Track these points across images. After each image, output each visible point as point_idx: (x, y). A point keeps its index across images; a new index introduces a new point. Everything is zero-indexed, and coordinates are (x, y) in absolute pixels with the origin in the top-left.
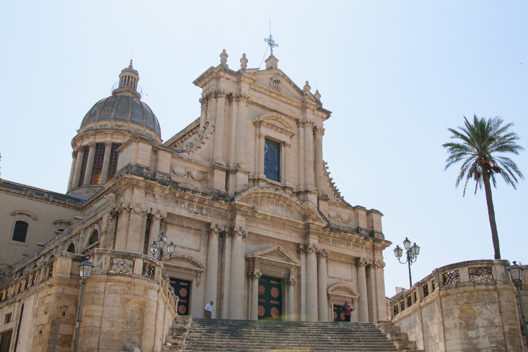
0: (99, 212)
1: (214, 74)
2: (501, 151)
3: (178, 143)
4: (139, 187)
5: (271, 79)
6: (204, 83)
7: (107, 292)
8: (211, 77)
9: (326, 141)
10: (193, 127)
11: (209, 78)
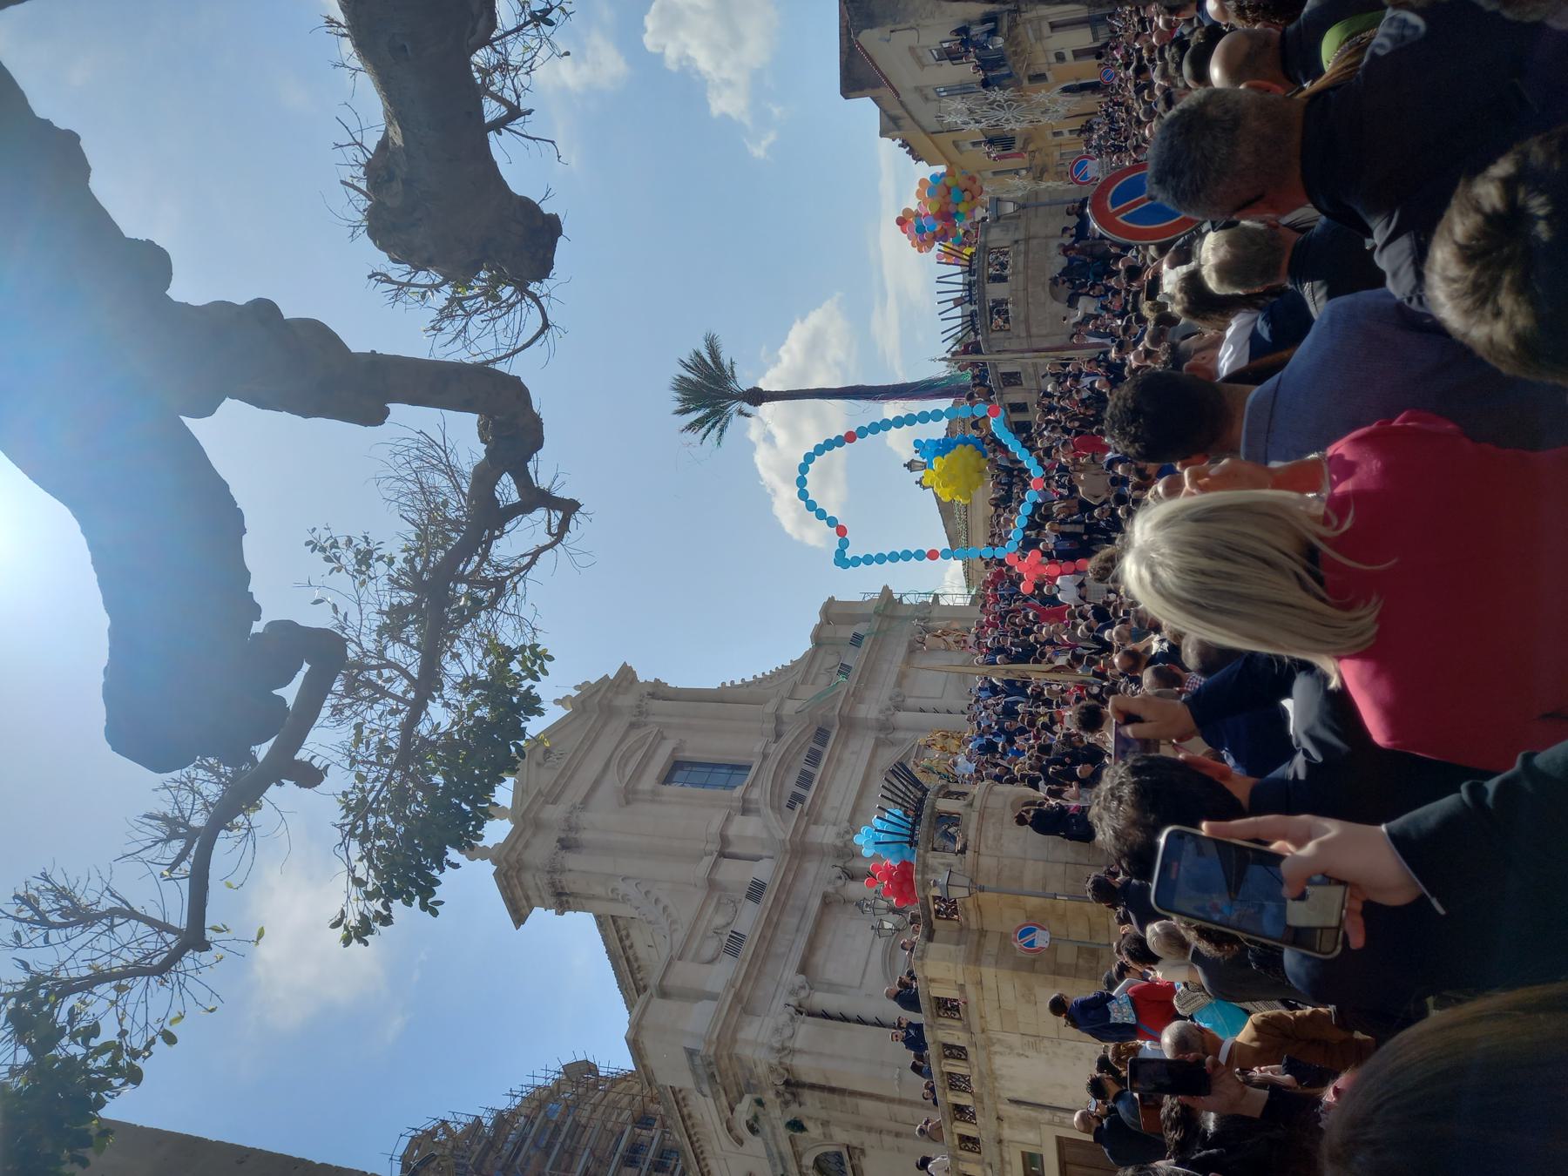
0: (778, 1147)
1: (509, 873)
2: (432, 1134)
3: (641, 979)
4: (735, 1031)
5: (539, 765)
6: (524, 902)
8: (516, 881)
9: (677, 679)
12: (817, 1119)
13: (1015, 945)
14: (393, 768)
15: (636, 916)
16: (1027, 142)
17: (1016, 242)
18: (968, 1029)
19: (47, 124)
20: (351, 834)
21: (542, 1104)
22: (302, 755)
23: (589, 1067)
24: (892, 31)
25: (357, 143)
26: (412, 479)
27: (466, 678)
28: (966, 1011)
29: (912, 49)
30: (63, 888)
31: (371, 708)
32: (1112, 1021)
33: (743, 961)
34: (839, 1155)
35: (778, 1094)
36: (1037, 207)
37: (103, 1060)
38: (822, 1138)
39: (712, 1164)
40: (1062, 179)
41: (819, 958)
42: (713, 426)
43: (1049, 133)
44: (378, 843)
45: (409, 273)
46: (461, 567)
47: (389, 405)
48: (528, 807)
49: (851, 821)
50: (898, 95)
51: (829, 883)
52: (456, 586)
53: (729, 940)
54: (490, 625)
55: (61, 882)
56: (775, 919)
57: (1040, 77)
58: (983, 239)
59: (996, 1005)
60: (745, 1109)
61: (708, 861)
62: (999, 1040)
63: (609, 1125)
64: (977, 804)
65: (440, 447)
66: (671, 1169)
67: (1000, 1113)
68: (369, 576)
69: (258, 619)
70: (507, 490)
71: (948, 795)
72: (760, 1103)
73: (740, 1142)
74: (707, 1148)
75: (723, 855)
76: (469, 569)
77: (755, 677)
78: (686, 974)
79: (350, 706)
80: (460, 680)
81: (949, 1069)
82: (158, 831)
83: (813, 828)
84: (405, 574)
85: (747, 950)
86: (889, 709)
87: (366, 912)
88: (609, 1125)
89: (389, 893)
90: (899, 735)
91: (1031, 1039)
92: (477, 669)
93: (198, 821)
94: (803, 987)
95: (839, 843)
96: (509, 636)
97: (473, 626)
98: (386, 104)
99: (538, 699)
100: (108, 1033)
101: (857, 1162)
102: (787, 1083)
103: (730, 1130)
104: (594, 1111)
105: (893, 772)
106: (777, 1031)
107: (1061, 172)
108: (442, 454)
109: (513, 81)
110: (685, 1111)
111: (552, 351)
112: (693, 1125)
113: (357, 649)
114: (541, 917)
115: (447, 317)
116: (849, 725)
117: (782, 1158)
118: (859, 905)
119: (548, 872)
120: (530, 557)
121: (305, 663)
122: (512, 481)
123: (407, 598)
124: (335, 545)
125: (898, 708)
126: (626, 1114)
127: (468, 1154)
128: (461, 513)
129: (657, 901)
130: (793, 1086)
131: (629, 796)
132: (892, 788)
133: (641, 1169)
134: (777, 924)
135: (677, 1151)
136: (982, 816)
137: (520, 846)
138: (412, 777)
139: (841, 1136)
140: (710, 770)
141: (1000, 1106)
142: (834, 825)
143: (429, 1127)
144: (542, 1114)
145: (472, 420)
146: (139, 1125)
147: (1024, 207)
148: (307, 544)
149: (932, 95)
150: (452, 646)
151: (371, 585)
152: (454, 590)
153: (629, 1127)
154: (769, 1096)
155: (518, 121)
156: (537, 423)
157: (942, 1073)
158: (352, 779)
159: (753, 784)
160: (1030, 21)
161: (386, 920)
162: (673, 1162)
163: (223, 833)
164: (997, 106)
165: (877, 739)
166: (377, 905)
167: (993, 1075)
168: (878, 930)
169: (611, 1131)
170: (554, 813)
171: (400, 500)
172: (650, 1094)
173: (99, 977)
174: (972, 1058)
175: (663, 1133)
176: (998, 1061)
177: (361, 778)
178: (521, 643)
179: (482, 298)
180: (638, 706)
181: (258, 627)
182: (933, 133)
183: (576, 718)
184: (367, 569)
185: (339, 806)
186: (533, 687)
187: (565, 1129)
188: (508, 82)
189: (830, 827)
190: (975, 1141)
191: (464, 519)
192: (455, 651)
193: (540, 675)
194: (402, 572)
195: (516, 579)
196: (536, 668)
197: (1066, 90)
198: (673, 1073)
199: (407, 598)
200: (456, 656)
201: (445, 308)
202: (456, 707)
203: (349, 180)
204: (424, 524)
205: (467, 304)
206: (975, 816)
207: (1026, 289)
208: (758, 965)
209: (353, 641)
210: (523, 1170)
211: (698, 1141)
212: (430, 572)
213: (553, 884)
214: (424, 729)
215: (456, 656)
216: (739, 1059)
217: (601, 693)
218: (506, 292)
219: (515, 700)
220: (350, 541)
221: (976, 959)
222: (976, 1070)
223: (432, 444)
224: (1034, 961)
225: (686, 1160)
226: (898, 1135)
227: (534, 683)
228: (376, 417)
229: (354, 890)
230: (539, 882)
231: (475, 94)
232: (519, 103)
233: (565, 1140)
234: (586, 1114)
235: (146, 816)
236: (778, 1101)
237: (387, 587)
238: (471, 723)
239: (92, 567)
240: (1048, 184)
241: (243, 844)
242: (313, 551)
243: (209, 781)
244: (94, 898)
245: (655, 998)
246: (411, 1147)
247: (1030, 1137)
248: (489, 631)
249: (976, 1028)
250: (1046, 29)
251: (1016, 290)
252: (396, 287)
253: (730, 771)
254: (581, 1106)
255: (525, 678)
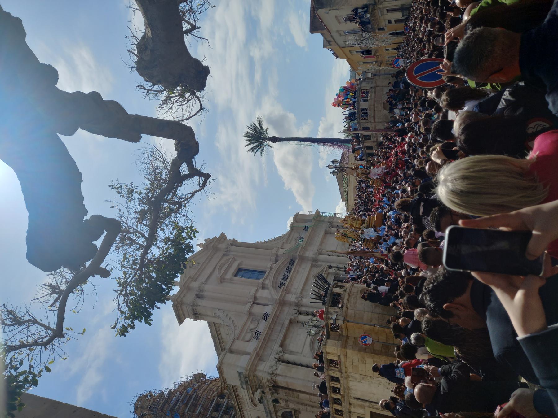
1: (178, 305)
2: (146, 396)
3: (223, 346)
4: (257, 366)
6: (183, 316)
7: (355, 309)
8: (180, 308)
10: (215, 329)
11: (180, 310)
12: (283, 399)
13: (360, 342)
14: (137, 270)
15: (222, 323)
16: (376, 52)
17: (372, 88)
18: (340, 371)
19: (9, 14)
20: (121, 294)
21: (185, 388)
22: (103, 265)
23: (203, 376)
24: (329, 10)
25: (134, 36)
26: (149, 163)
27: (166, 238)
28: (340, 365)
29: (336, 17)
30: (11, 310)
31: (130, 247)
32: (396, 376)
33: (260, 341)
34: (291, 412)
35: (270, 390)
36: (380, 75)
37: (22, 378)
38: (285, 406)
39: (245, 413)
40: (388, 66)
41: (287, 342)
42: (259, 149)
43: (384, 49)
44: (131, 298)
45: (152, 86)
46: (166, 197)
47: (141, 135)
48: (185, 282)
49: (301, 293)
50: (330, 33)
51: (292, 315)
52: (163, 204)
53: (255, 334)
54: (175, 219)
55: (10, 308)
56: (272, 327)
57: (383, 29)
58: (359, 86)
59: (351, 363)
60: (258, 394)
61: (249, 305)
62: (352, 376)
63: (209, 397)
64: (348, 290)
65: (160, 152)
66: (230, 414)
67: (351, 402)
68: (132, 198)
69: (86, 215)
70: (184, 169)
71: (338, 287)
72: (263, 392)
73: (255, 405)
74: (244, 407)
75: (254, 303)
76: (169, 197)
77: (269, 240)
78: (239, 345)
79: (122, 246)
80: (163, 238)
81: (333, 385)
82: (47, 290)
83: (287, 295)
84: (145, 198)
85: (262, 338)
86: (316, 254)
87: (125, 324)
88: (209, 397)
89: (133, 317)
90: (320, 263)
91: (364, 376)
92: (170, 235)
93: (63, 287)
94: (281, 352)
95: (296, 301)
96: (182, 223)
97: (169, 219)
98: (145, 20)
99: (192, 247)
100: (25, 367)
101: (297, 415)
102: (273, 386)
103: (252, 401)
104: (204, 391)
105: (318, 277)
106: (271, 367)
107: (388, 64)
108: (161, 154)
109: (193, 16)
110: (236, 393)
111: (203, 118)
112: (239, 398)
113: (126, 225)
114: (188, 321)
115: (165, 103)
116: (302, 259)
117: (270, 412)
118: (303, 324)
119: (192, 306)
120: (192, 194)
121: (105, 231)
122: (186, 166)
123: (146, 207)
124: (120, 187)
125: (320, 254)
126: (215, 393)
127: (158, 404)
128: (167, 177)
129: (230, 318)
130: (276, 387)
131: (222, 280)
132: (316, 282)
133: (220, 413)
134: (273, 329)
135: (233, 407)
136: (349, 295)
137: (182, 296)
138: (144, 273)
139: (292, 406)
140: (251, 272)
141: (351, 400)
142: (295, 294)
143: (145, 394)
144: (185, 391)
145: (172, 142)
146: (38, 396)
147: (375, 75)
148: (110, 186)
149: (343, 34)
150: (161, 226)
151: (132, 202)
152: (163, 205)
153: (216, 398)
154: (267, 390)
155: (194, 31)
156: (197, 144)
157: (330, 386)
158: (122, 274)
159: (266, 278)
160: (380, 8)
161: (133, 327)
162: (231, 411)
163: (71, 295)
164: (366, 39)
165: (312, 264)
166: (129, 322)
167: (349, 389)
168: (309, 333)
169: (210, 399)
170: (195, 285)
171: (144, 171)
172: (224, 387)
173: (23, 346)
174: (341, 382)
175: (228, 400)
176: (351, 384)
177: (125, 273)
178: (187, 226)
179: (178, 97)
180: (227, 248)
181: (87, 218)
182: (342, 47)
183: (204, 251)
184: (132, 196)
185: (117, 282)
186: (190, 242)
187: (193, 397)
188: (192, 17)
189: (293, 295)
190: (341, 411)
191: (168, 179)
192: (162, 227)
193: (193, 238)
194: (144, 197)
195: (186, 202)
196: (192, 235)
197: (391, 34)
198: (233, 380)
199: (146, 207)
200: (163, 229)
201: (164, 100)
202: (161, 248)
203: (131, 50)
204: (153, 180)
205: (172, 99)
206: (347, 295)
207: (374, 105)
208: (265, 344)
209: (124, 222)
210: (178, 411)
211: (240, 404)
212: (154, 198)
213: (193, 310)
214: (149, 256)
215: (163, 229)
216: (257, 377)
217: (214, 242)
218: (188, 95)
219: (183, 247)
220: (127, 186)
221: (345, 346)
222: (342, 386)
223: (158, 150)
224: (366, 348)
225: (236, 411)
226: (312, 407)
227: (191, 241)
228: (136, 139)
229: (121, 316)
230: (188, 309)
231: (179, 18)
232: (195, 24)
233: (193, 401)
234: (201, 392)
235: (44, 285)
236: (270, 392)
237: (138, 203)
238: (166, 254)
239: (22, 192)
240: (383, 68)
241: (79, 297)
242: (112, 189)
243: (67, 273)
244: (23, 314)
245: (228, 353)
246: (138, 400)
247: (361, 411)
248: (175, 221)
249: (343, 371)
250: (385, 11)
251: (371, 105)
252: (146, 91)
253: (258, 273)
254: (200, 389)
255: (187, 239)
